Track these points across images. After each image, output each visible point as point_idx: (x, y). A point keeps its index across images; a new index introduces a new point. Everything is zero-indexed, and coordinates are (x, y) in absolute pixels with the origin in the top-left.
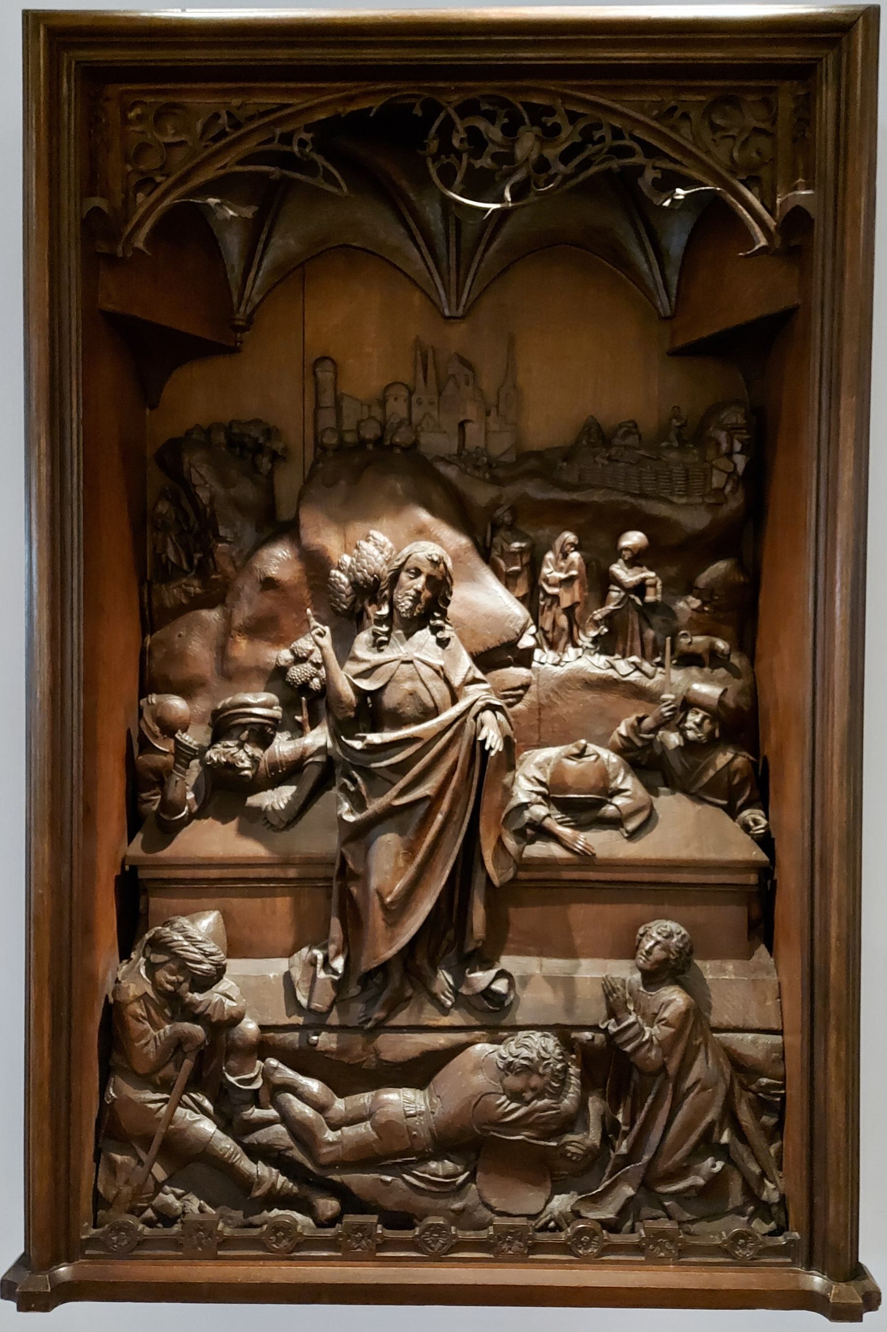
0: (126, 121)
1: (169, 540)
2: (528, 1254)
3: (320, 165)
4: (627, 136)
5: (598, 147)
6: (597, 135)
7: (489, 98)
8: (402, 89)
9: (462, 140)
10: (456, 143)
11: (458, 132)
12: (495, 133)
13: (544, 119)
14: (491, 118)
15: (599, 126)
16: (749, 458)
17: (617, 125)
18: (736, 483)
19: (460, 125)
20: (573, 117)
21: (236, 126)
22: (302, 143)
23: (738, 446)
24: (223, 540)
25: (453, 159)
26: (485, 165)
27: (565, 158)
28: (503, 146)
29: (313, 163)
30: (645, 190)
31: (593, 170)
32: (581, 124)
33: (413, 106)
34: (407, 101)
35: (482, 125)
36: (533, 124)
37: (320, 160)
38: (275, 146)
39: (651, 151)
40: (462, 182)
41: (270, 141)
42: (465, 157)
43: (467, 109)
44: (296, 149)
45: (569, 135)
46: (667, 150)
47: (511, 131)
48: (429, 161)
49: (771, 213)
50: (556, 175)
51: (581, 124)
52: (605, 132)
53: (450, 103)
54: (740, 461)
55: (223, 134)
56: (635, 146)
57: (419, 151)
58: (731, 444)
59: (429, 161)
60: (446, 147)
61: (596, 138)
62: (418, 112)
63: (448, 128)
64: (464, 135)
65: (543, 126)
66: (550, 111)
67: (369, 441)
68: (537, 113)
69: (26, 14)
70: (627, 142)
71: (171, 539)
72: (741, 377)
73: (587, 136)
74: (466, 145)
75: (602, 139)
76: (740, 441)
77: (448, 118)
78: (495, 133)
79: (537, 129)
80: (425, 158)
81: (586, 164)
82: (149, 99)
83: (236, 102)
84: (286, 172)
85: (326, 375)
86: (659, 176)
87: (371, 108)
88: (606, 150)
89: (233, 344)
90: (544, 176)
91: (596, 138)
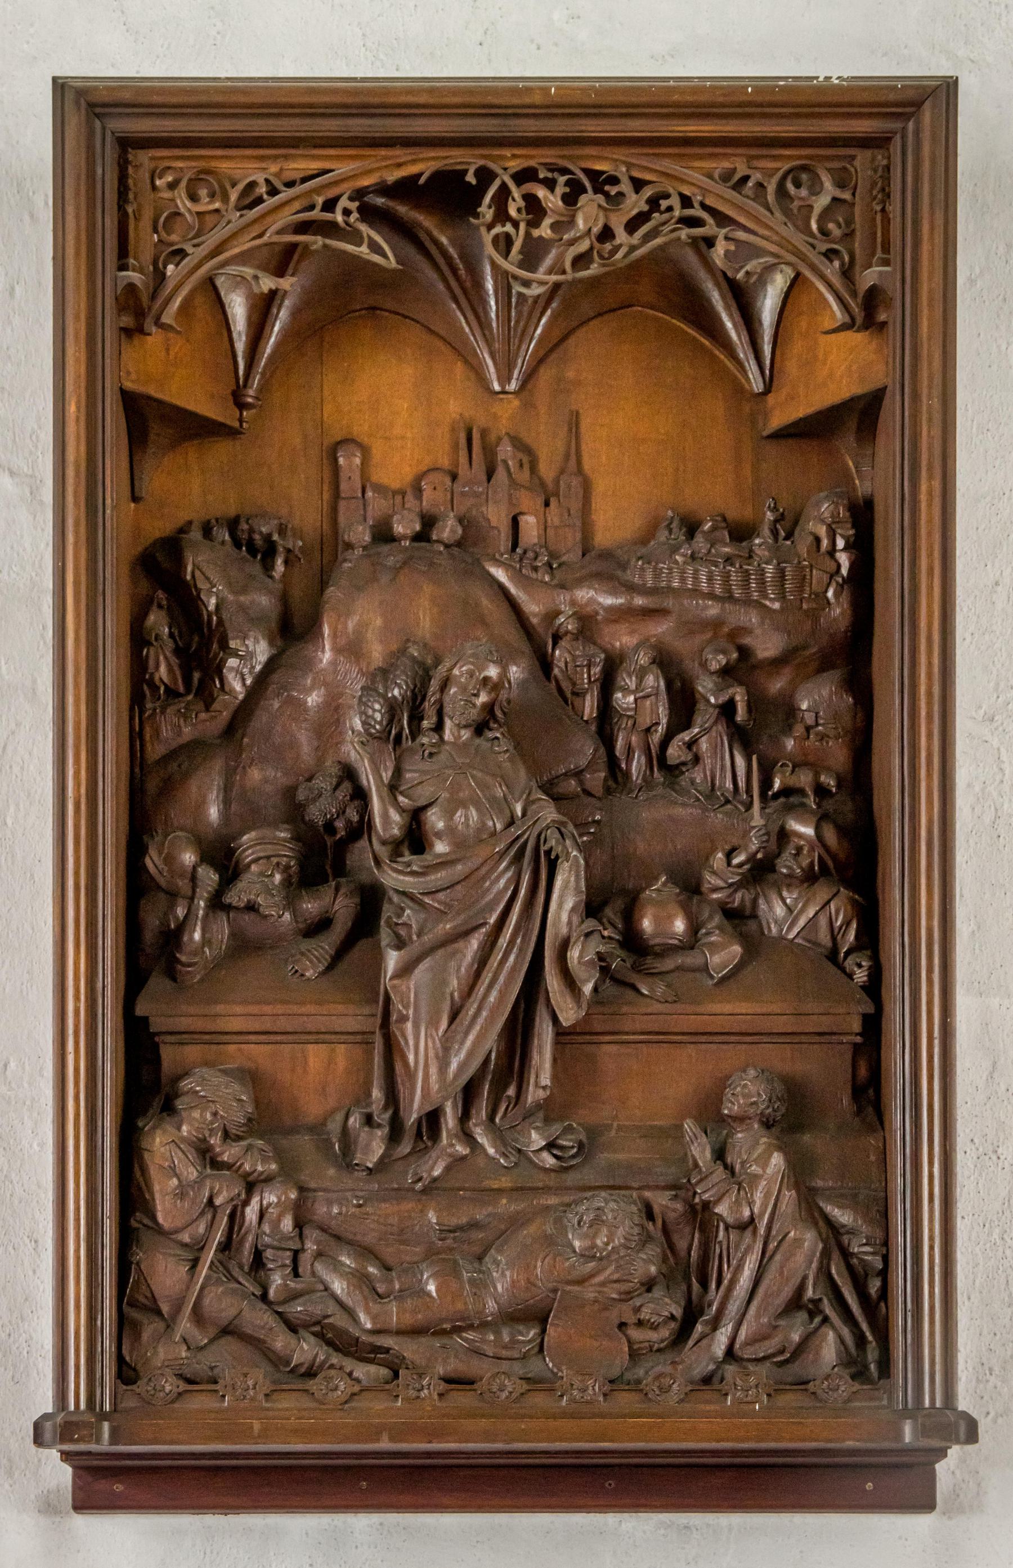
0: (154, 188)
1: (161, 658)
2: (819, 510)
3: (365, 235)
4: (696, 205)
5: (666, 216)
6: (664, 204)
7: (551, 168)
8: (456, 157)
9: (519, 210)
10: (513, 212)
11: (514, 200)
12: (552, 200)
13: (607, 188)
14: (550, 185)
15: (667, 196)
16: (853, 557)
17: (687, 193)
18: (840, 587)
19: (516, 193)
20: (638, 185)
21: (273, 192)
22: (347, 212)
23: (840, 543)
24: (235, 654)
25: (509, 228)
26: (544, 235)
27: (631, 227)
28: (562, 215)
29: (357, 233)
30: (717, 262)
31: (658, 241)
32: (648, 192)
33: (466, 171)
34: (459, 167)
35: (541, 193)
36: (596, 192)
37: (364, 228)
38: (316, 214)
39: (722, 219)
40: (521, 252)
41: (312, 207)
42: (522, 226)
43: (524, 176)
44: (340, 218)
45: (635, 203)
46: (742, 220)
47: (570, 199)
48: (483, 230)
49: (854, 294)
50: (620, 246)
51: (648, 192)
52: (675, 201)
53: (505, 169)
54: (844, 560)
55: (260, 200)
56: (705, 215)
57: (472, 220)
58: (833, 543)
59: (483, 230)
60: (502, 215)
61: (663, 208)
62: (471, 178)
63: (503, 194)
64: (522, 203)
65: (607, 195)
66: (614, 180)
67: (404, 537)
68: (600, 181)
69: (60, 86)
70: (697, 212)
71: (166, 658)
72: (381, 1151)
73: (654, 203)
74: (524, 215)
75: (670, 209)
76: (842, 536)
77: (504, 186)
78: (552, 200)
79: (600, 198)
80: (477, 228)
81: (654, 233)
82: (180, 164)
83: (274, 168)
84: (328, 241)
85: (349, 462)
86: (733, 248)
87: (420, 175)
88: (673, 221)
89: (237, 424)
90: (608, 246)
91: (663, 208)
